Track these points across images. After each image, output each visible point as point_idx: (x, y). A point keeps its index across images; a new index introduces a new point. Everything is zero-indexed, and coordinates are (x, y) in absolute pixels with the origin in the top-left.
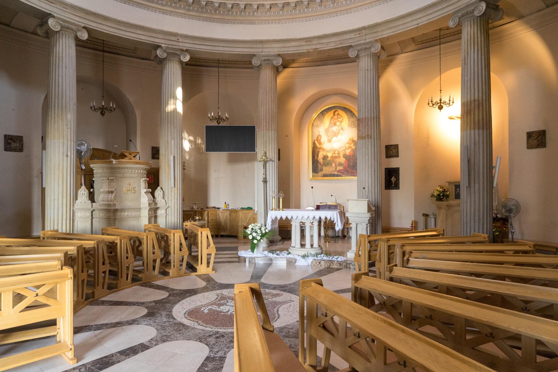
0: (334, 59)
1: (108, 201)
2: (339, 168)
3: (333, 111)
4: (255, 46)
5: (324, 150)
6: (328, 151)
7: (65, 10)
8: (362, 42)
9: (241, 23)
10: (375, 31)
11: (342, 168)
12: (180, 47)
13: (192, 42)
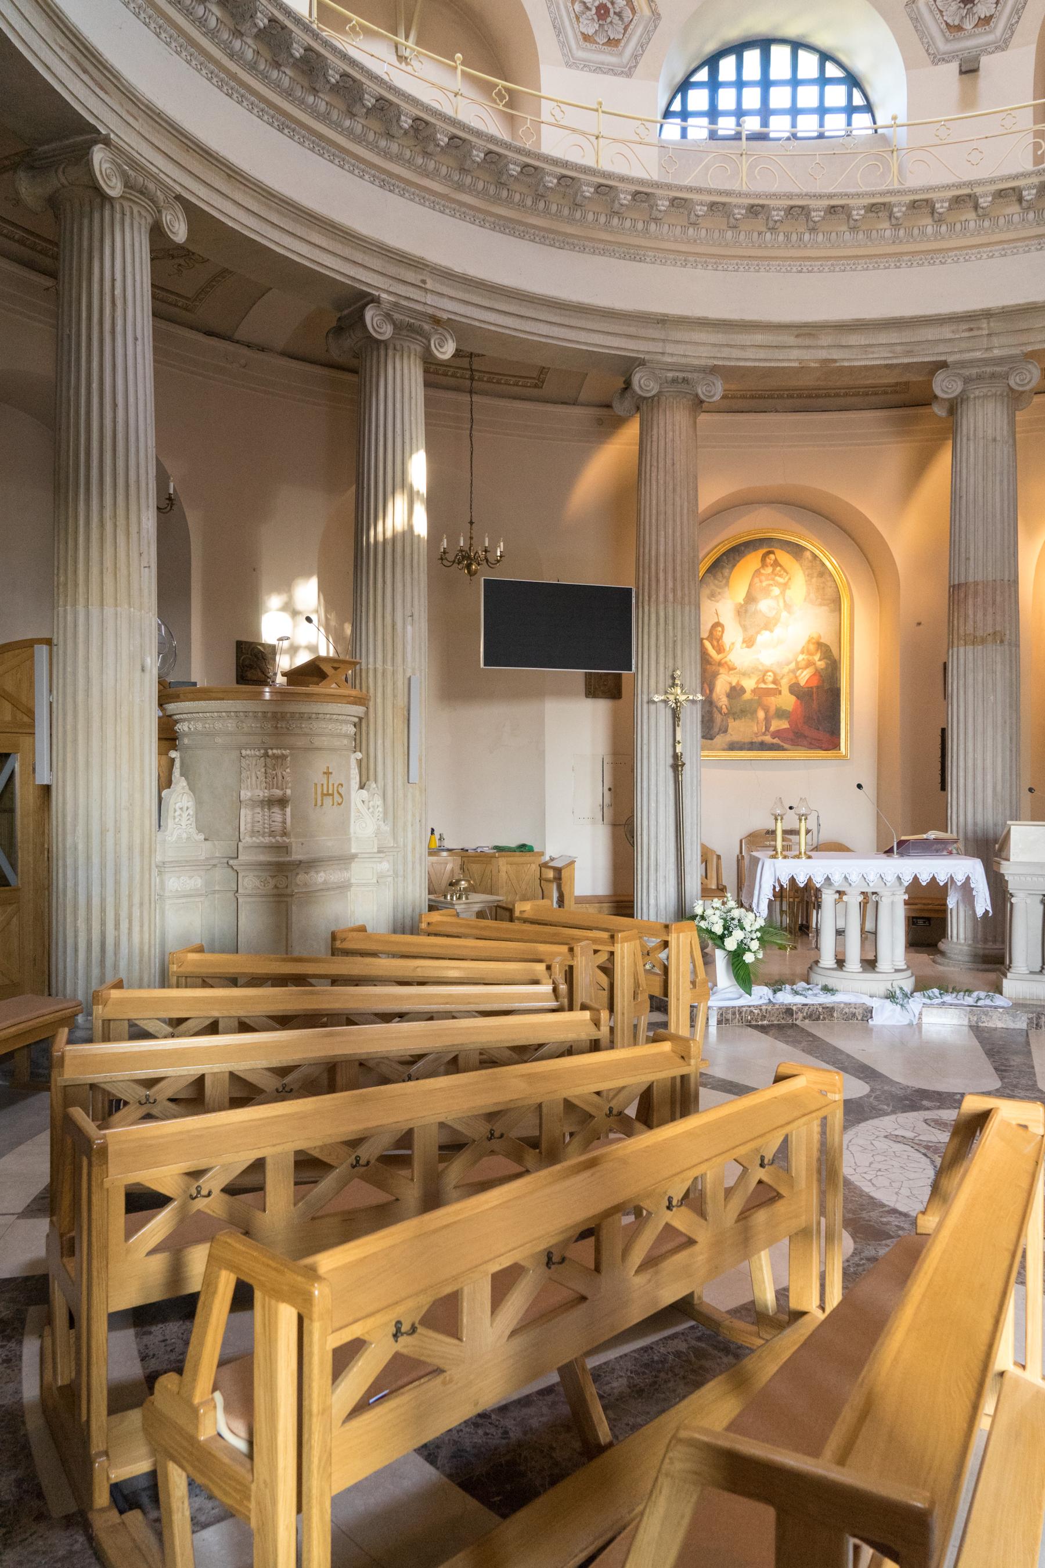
0: (791, 397)
1: (272, 834)
2: (777, 725)
3: (762, 552)
4: (642, 332)
5: (731, 668)
6: (744, 674)
7: (131, 120)
8: (978, 355)
9: (603, 253)
10: (1023, 325)
11: (784, 725)
12: (430, 311)
13: (460, 295)
